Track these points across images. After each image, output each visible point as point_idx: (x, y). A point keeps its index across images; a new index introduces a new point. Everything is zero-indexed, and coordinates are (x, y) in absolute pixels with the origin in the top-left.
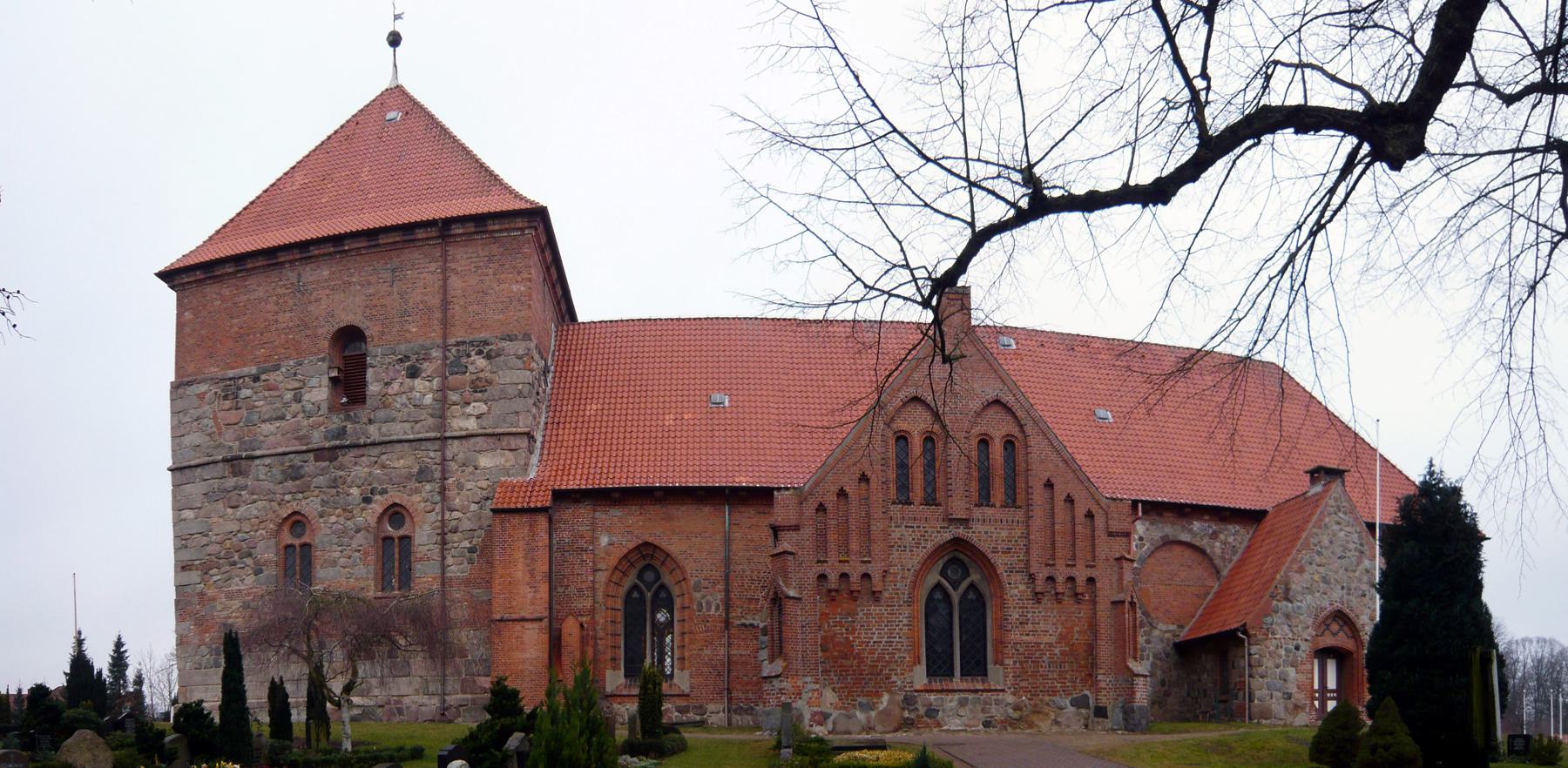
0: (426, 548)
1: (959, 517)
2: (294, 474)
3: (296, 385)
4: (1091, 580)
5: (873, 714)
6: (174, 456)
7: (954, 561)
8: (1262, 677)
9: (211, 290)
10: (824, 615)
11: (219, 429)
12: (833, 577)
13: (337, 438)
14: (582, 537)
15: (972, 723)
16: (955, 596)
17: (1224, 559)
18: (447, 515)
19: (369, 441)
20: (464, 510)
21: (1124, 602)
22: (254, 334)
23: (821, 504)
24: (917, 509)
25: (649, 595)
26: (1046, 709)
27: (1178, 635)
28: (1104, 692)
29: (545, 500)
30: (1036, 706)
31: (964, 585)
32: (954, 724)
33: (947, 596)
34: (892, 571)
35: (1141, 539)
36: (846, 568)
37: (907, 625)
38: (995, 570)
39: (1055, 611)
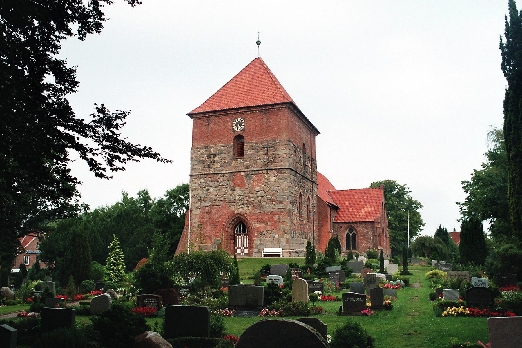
31: (353, 233)
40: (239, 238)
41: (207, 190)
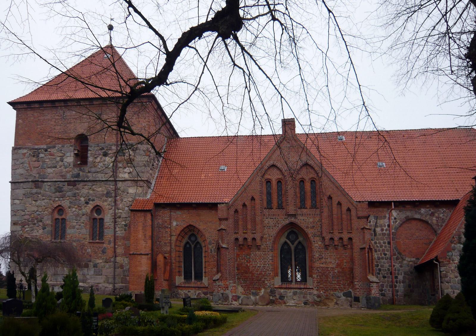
0: (109, 224)
1: (292, 213)
2: (59, 190)
3: (61, 155)
4: (350, 239)
5: (258, 297)
6: (12, 177)
7: (292, 232)
8: (448, 283)
9: (30, 113)
10: (238, 255)
11: (31, 168)
12: (241, 239)
13: (76, 177)
14: (166, 222)
15: (299, 302)
16: (293, 247)
17: (438, 225)
18: (117, 211)
19: (88, 179)
20: (123, 209)
21: (365, 248)
22: (46, 133)
23: (236, 210)
24: (274, 211)
25: (193, 246)
26: (332, 297)
27: (417, 263)
28: (358, 290)
29: (151, 207)
30: (327, 296)
31: (296, 242)
32: (291, 303)
33: (290, 248)
34: (265, 237)
35: (395, 219)
36: (246, 236)
37: (271, 260)
38: (308, 236)
39: (335, 253)
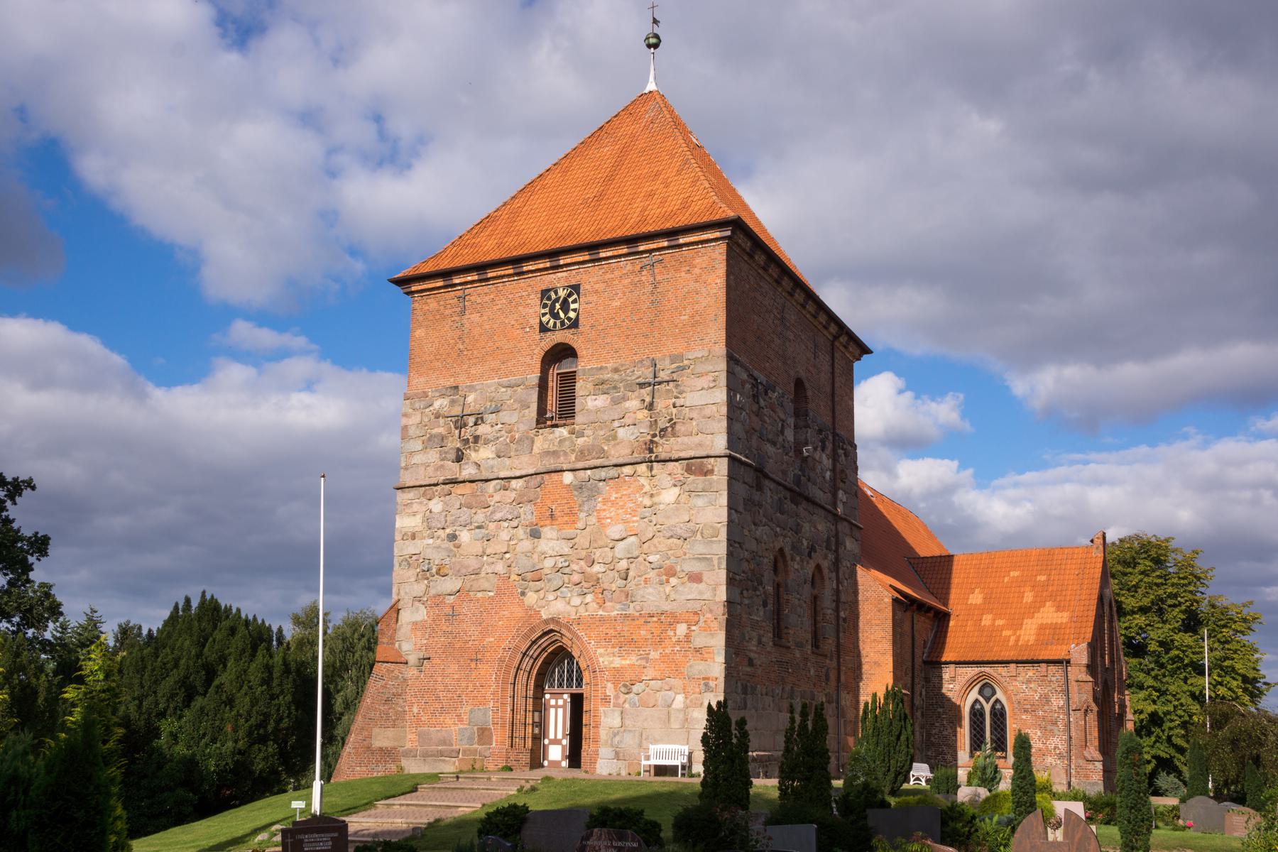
40: (556, 707)
41: (453, 537)
